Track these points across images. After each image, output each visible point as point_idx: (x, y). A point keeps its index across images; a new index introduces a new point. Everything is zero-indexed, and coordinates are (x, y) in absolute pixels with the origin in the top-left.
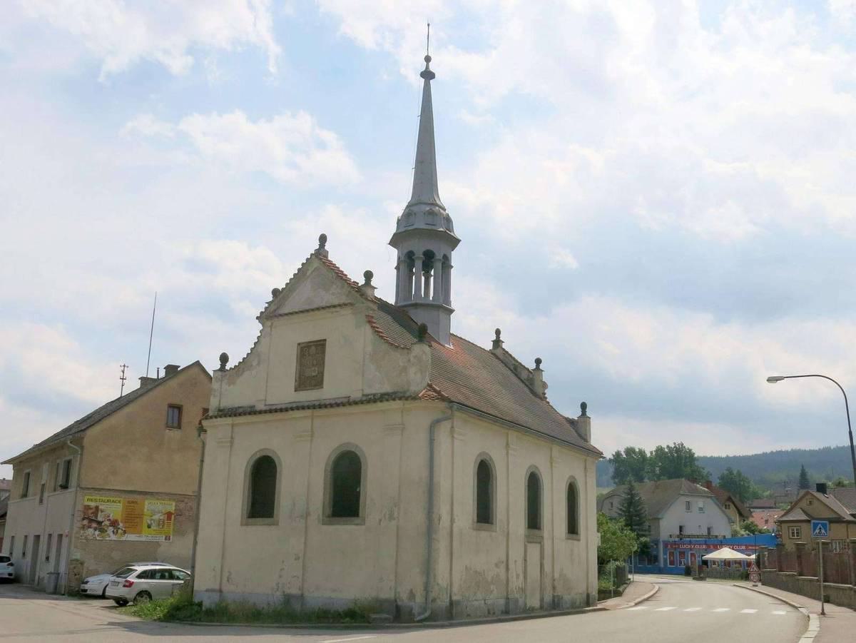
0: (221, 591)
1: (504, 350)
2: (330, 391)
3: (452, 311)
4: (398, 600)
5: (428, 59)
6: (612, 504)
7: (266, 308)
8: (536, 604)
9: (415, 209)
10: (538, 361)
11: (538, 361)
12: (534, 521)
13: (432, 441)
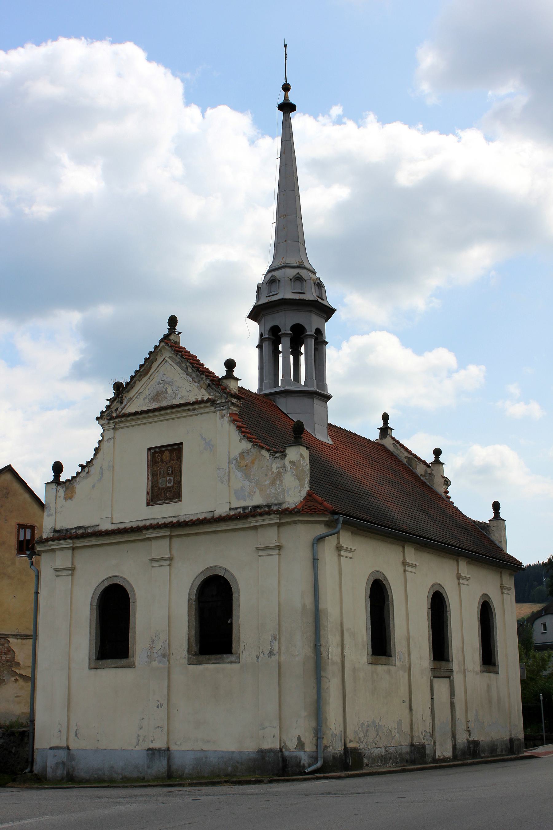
0: (68, 748)
1: (394, 439)
2: (189, 507)
3: (329, 397)
4: (284, 750)
5: (286, 88)
6: (545, 625)
7: (108, 407)
8: (449, 753)
9: (276, 274)
10: (437, 452)
11: (437, 452)
12: (440, 648)
13: (315, 560)
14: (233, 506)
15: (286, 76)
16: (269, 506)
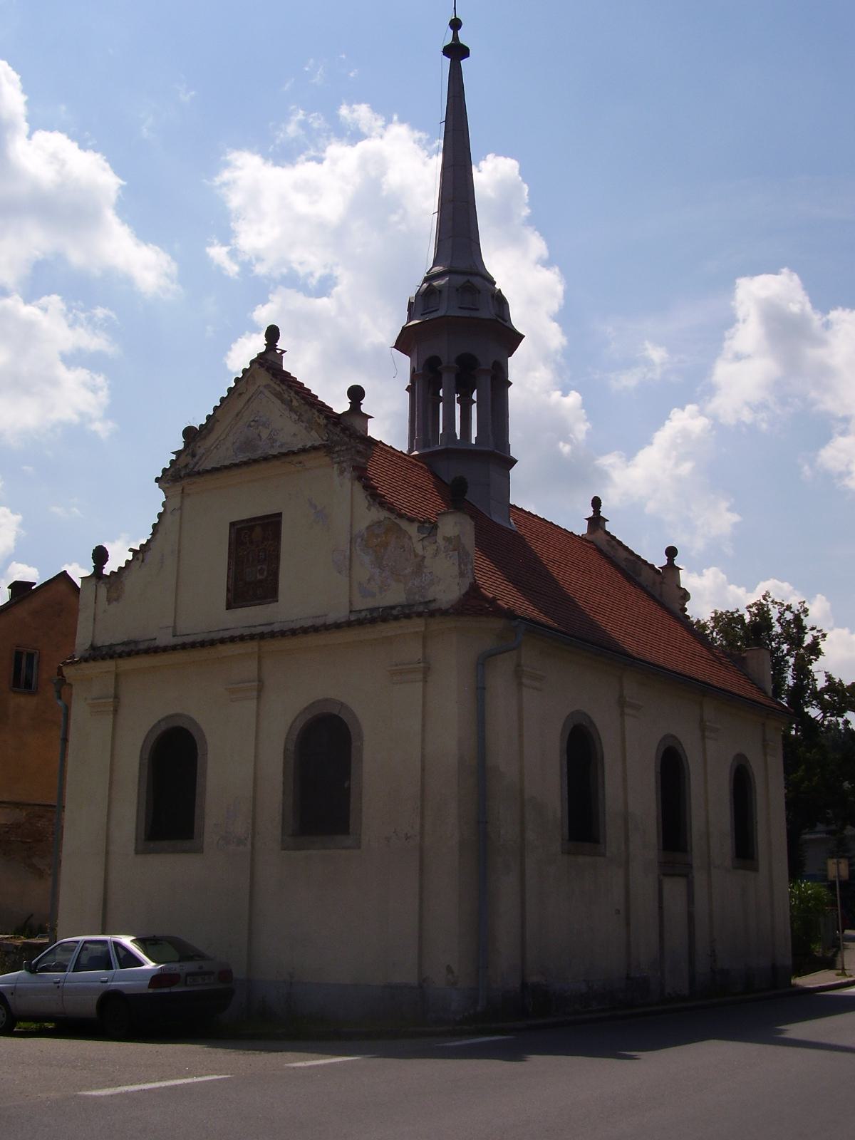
1: (608, 533)
5: (456, 24)
14: (358, 607)
15: (455, 8)
16: (410, 606)
